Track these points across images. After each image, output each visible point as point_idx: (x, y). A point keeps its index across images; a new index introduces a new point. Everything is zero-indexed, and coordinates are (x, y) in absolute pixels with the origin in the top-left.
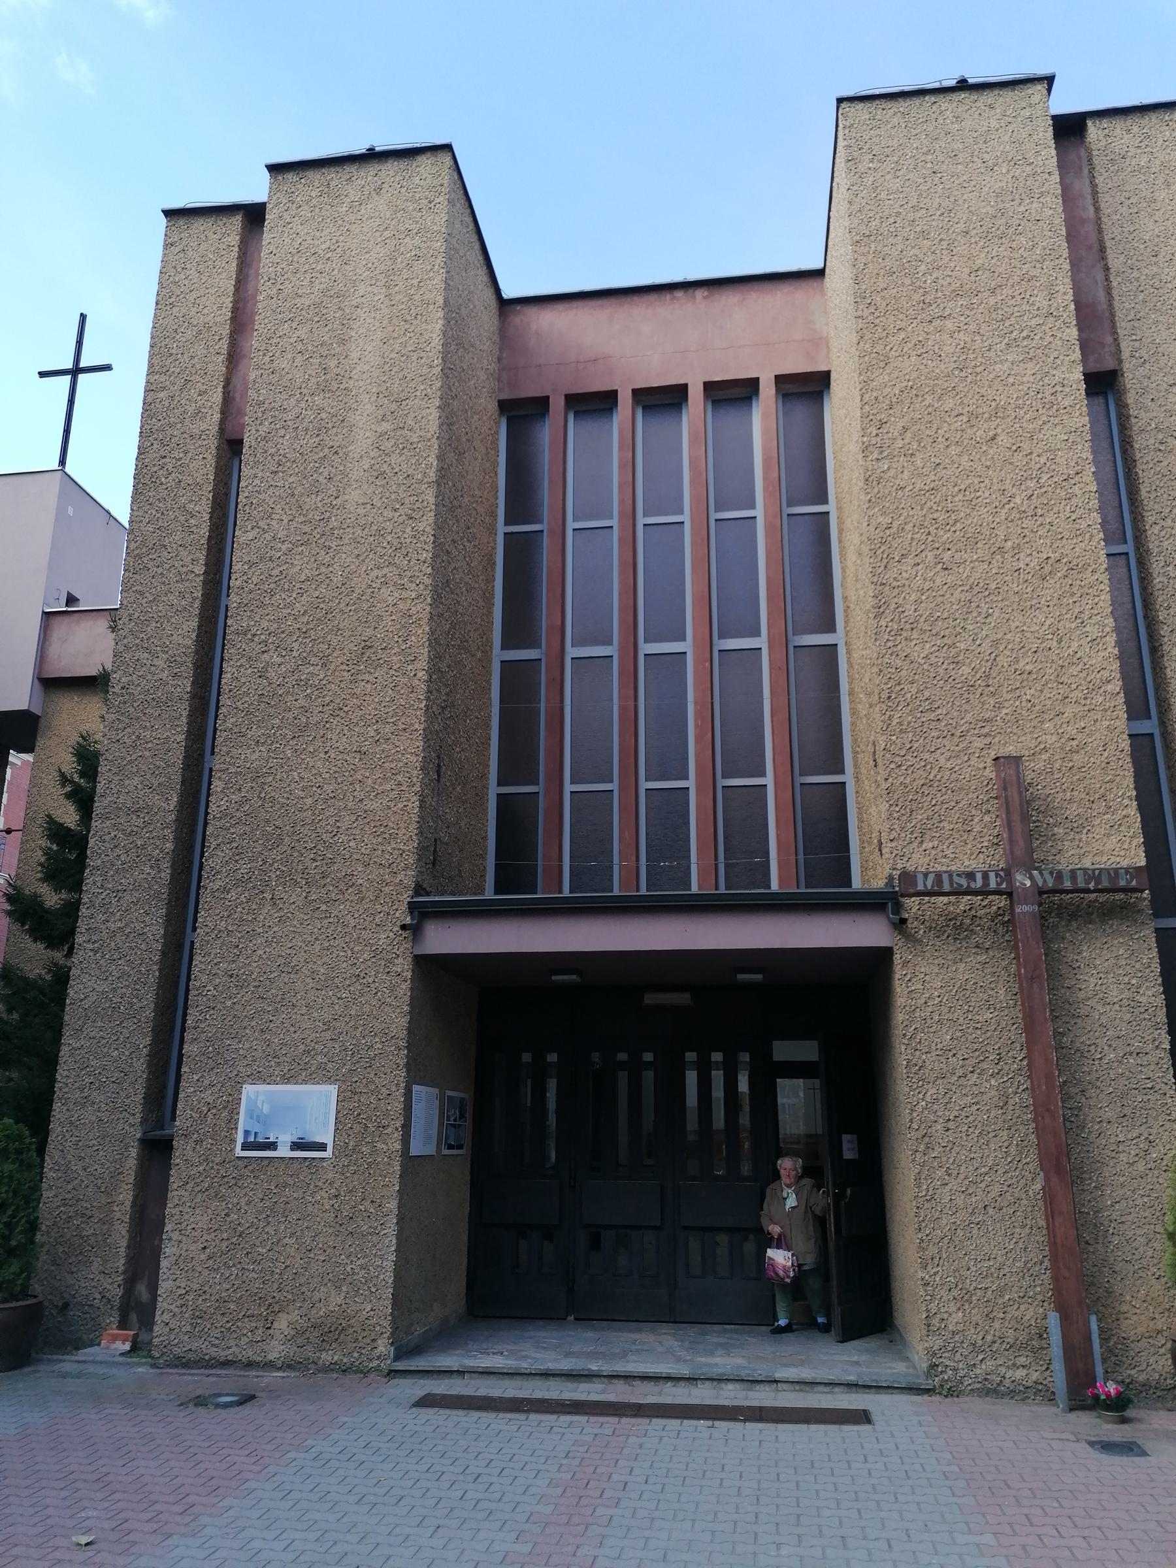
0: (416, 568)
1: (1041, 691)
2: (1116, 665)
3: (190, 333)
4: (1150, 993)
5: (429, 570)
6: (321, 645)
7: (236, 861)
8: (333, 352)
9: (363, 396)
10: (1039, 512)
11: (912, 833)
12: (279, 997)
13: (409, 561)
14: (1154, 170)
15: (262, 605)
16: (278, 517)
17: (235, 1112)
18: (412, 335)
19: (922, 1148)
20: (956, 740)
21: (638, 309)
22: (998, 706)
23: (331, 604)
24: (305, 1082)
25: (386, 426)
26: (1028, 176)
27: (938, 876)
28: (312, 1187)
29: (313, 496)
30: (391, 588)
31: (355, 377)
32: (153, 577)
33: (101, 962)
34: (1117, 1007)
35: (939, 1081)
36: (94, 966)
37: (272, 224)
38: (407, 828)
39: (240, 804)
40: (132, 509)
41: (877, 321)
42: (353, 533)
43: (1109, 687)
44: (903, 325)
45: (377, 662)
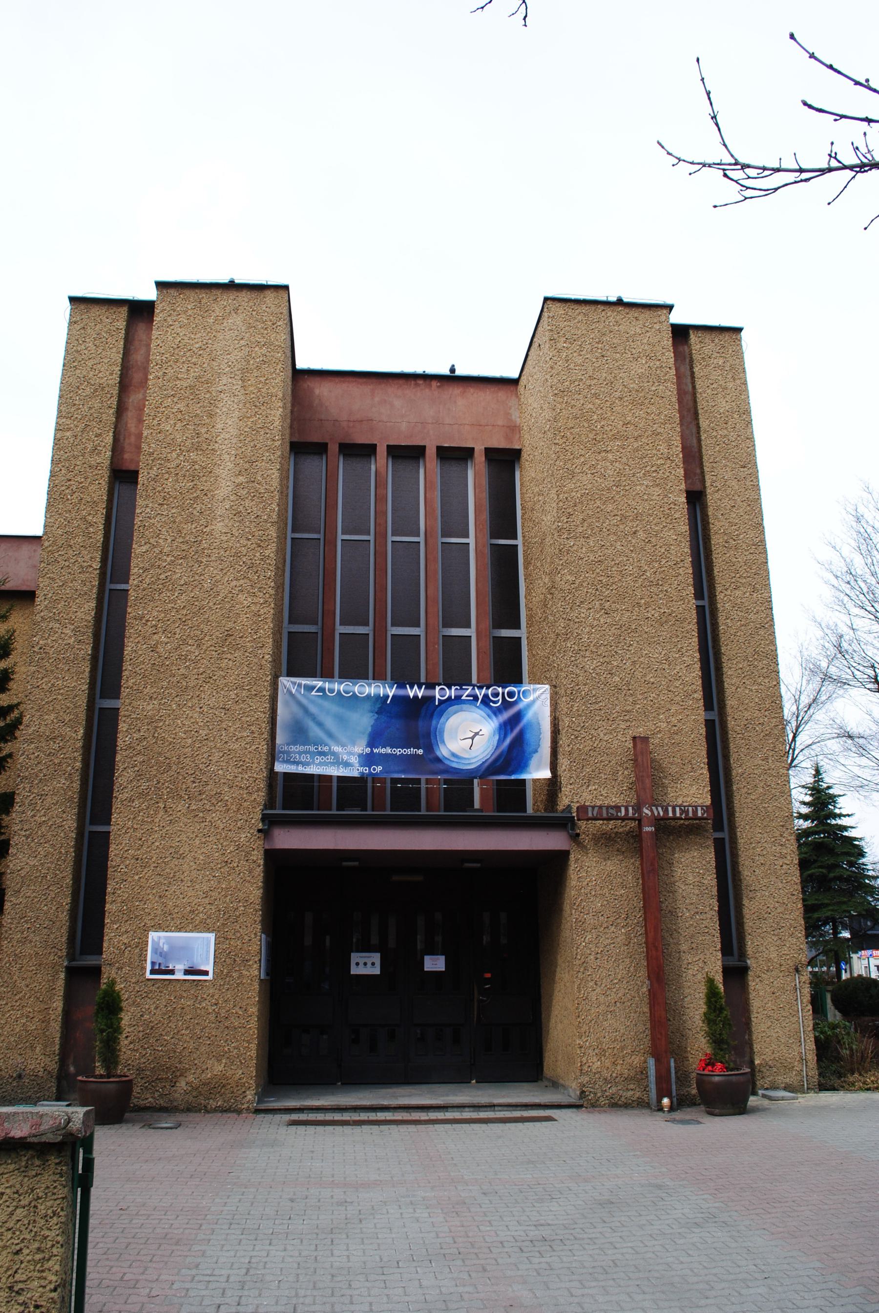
0: (264, 582)
1: (658, 695)
2: (700, 682)
3: (88, 391)
4: (709, 878)
5: (272, 584)
6: (196, 631)
7: (138, 780)
8: (203, 422)
9: (225, 456)
10: (660, 583)
11: (583, 780)
12: (172, 874)
13: (258, 577)
14: (727, 369)
15: (153, 600)
16: (164, 537)
17: (144, 949)
18: (261, 416)
19: (582, 970)
20: (610, 722)
21: (392, 390)
22: (634, 703)
23: (203, 603)
24: (191, 931)
25: (241, 479)
26: (657, 367)
27: (600, 807)
28: (199, 998)
29: (189, 524)
30: (246, 595)
31: (220, 442)
32: (62, 568)
33: (32, 844)
34: (692, 887)
35: (593, 931)
36: (26, 847)
37: (159, 325)
38: (259, 763)
39: (140, 740)
40: (46, 517)
41: (567, 448)
42: (219, 553)
43: (696, 695)
44: (583, 452)
45: (236, 646)
